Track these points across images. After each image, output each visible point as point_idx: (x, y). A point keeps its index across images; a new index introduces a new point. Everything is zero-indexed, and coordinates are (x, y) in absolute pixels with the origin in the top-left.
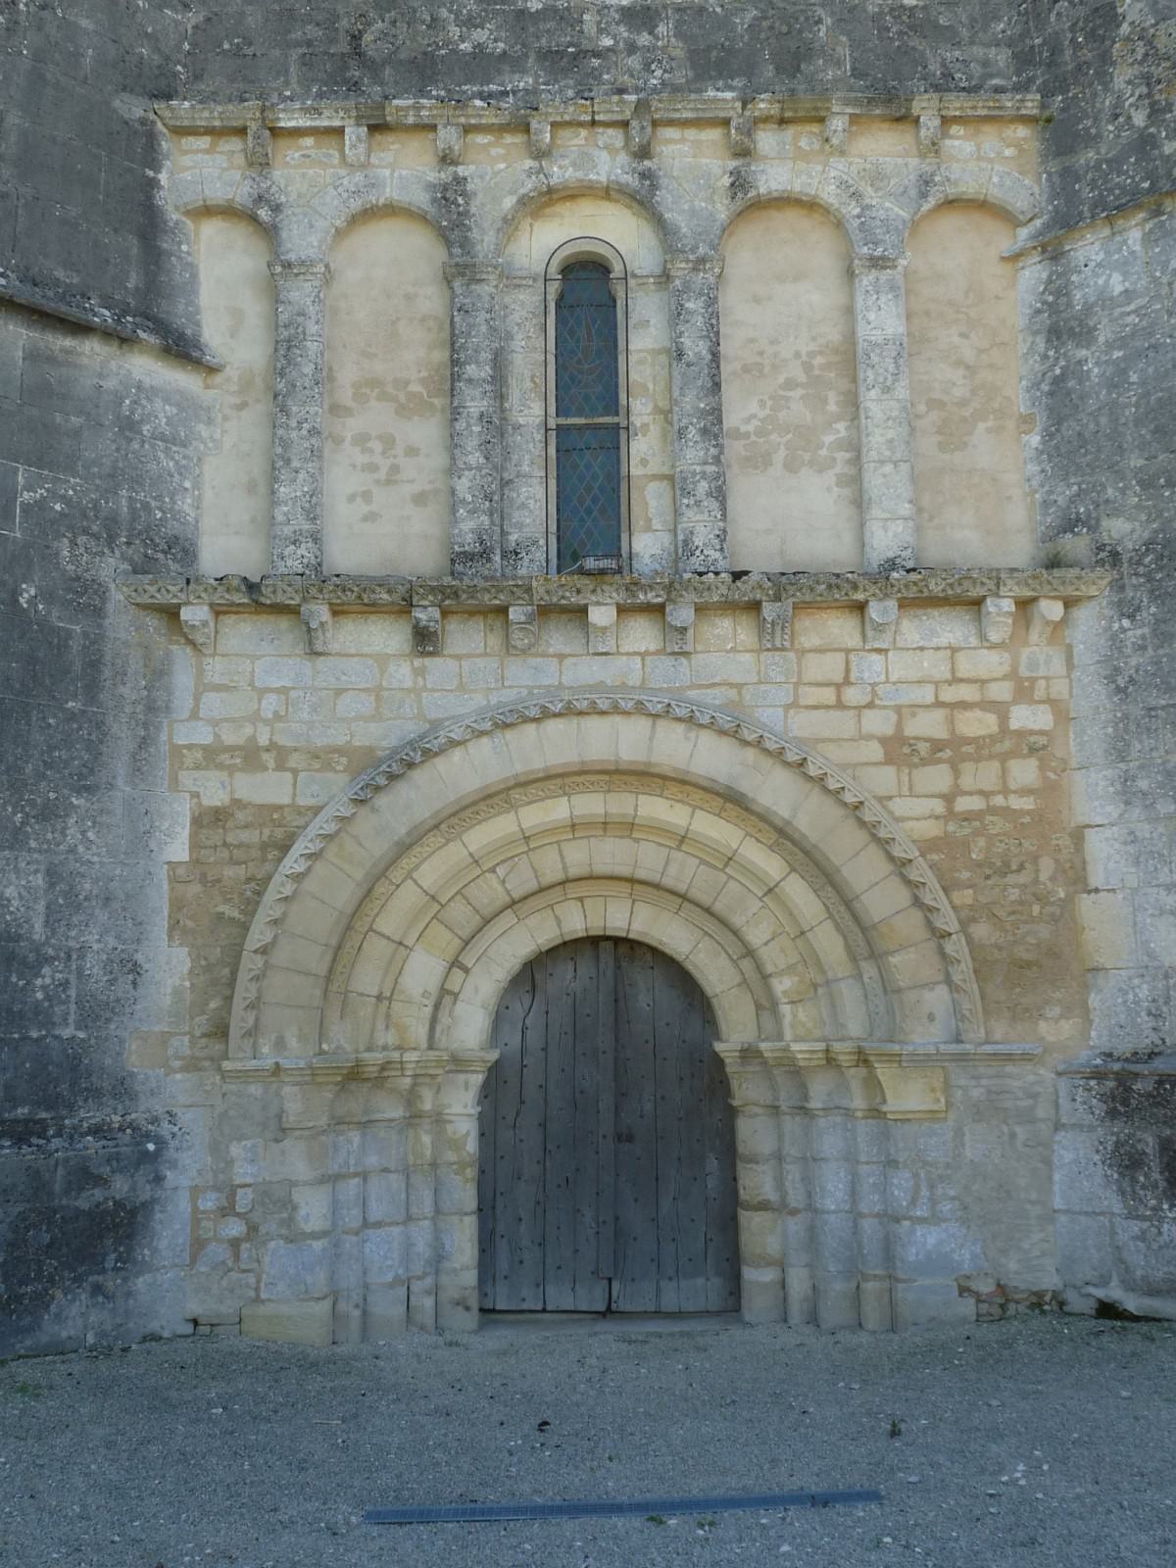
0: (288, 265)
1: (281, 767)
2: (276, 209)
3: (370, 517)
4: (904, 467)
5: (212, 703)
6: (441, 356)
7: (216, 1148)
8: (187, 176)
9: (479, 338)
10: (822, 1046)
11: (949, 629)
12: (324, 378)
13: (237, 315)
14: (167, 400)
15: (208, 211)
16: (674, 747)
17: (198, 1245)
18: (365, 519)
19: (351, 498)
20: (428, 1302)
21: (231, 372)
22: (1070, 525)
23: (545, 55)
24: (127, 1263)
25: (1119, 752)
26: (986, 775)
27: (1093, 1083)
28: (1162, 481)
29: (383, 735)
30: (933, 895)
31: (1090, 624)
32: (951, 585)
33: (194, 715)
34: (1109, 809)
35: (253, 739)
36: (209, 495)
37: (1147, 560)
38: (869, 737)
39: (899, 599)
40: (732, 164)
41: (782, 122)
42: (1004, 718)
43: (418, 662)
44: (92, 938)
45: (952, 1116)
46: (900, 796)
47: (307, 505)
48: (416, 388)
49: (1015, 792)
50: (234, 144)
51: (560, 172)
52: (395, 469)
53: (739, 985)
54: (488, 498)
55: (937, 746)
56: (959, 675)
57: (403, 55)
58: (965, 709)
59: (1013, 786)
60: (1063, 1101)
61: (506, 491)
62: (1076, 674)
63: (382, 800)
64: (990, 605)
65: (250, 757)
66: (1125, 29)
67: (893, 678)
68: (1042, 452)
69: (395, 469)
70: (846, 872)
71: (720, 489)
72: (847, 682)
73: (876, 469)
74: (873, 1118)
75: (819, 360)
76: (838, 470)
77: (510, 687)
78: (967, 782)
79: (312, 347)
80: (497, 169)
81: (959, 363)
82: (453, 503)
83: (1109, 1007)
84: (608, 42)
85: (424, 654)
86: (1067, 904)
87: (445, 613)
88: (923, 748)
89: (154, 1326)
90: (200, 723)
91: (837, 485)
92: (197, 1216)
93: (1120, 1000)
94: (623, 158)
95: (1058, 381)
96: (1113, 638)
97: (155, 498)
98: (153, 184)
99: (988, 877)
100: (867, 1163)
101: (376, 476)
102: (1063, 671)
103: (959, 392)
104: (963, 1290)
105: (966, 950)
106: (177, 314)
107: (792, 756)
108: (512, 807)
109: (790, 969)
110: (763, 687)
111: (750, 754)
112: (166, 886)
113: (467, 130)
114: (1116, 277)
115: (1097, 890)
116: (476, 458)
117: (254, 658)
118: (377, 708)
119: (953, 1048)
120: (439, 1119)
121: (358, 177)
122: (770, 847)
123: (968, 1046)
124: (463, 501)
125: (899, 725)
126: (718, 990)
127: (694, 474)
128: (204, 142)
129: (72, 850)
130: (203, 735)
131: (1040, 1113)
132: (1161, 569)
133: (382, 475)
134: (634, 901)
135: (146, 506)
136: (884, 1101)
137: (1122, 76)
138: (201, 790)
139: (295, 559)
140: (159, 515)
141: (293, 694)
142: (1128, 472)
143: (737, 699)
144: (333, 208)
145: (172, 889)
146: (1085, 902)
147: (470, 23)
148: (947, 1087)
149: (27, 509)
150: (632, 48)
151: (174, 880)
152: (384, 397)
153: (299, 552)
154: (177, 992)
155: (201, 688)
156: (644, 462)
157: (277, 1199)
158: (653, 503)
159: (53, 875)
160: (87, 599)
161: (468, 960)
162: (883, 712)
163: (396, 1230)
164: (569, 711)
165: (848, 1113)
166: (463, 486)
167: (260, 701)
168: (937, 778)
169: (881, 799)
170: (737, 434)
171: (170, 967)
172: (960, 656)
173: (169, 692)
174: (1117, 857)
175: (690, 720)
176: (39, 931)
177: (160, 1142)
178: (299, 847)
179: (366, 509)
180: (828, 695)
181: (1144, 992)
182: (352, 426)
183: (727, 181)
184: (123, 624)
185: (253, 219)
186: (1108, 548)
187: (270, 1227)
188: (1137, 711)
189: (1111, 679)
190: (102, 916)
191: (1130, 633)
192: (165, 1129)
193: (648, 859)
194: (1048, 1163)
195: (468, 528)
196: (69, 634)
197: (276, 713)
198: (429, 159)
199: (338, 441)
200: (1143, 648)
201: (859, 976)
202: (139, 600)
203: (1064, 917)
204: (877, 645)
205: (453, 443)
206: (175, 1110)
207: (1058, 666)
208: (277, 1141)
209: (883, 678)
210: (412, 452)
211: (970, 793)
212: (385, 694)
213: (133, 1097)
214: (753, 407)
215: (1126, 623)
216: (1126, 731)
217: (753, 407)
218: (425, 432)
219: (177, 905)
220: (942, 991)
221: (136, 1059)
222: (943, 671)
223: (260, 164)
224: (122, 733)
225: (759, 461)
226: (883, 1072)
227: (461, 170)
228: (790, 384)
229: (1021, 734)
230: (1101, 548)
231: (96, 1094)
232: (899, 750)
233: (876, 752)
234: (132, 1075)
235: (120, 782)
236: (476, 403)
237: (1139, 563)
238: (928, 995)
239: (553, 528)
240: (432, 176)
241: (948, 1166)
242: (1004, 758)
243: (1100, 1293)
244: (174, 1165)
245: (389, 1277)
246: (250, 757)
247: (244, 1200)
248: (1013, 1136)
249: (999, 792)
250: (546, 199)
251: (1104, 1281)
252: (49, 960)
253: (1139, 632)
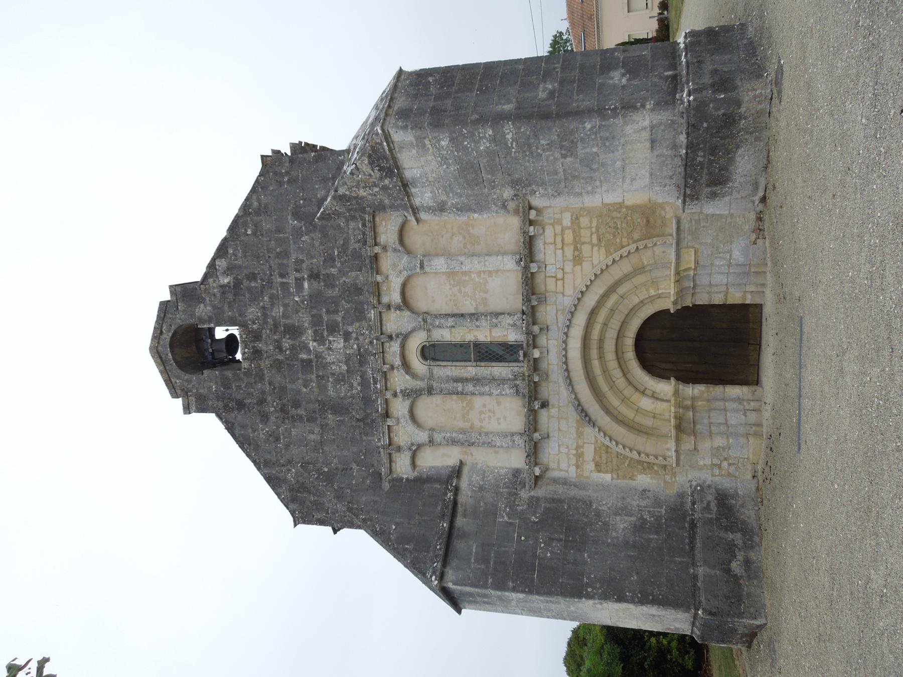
0: (430, 441)
1: (583, 447)
2: (412, 444)
3: (505, 418)
4: (486, 258)
5: (564, 466)
6: (454, 397)
7: (700, 469)
8: (403, 469)
9: (450, 386)
11: (539, 245)
12: (463, 431)
13: (444, 455)
14: (472, 477)
15: (414, 464)
16: (577, 332)
17: (729, 475)
19: (499, 424)
20: (752, 404)
21: (462, 458)
22: (504, 207)
23: (361, 366)
24: (735, 496)
26: (585, 233)
29: (573, 416)
30: (624, 251)
33: (567, 471)
36: (499, 465)
38: (573, 270)
40: (392, 310)
41: (379, 295)
42: (568, 228)
44: (635, 503)
45: (697, 246)
48: (465, 404)
50: (394, 456)
51: (397, 362)
52: (490, 411)
54: (499, 385)
55: (576, 249)
57: (363, 406)
60: (693, 211)
63: (593, 418)
65: (579, 456)
66: (347, 193)
69: (490, 411)
70: (616, 278)
72: (555, 277)
75: (452, 282)
78: (588, 240)
79: (454, 435)
80: (399, 380)
81: (451, 238)
82: (501, 394)
84: (355, 346)
85: (548, 405)
86: (628, 208)
87: (536, 399)
88: (577, 253)
89: (754, 489)
92: (721, 475)
94: (392, 343)
95: (458, 209)
98: (407, 479)
103: (461, 239)
104: (755, 243)
106: (445, 473)
108: (594, 378)
109: (647, 290)
111: (579, 307)
113: (386, 389)
114: (426, 195)
116: (487, 389)
120: (693, 398)
121: (402, 421)
128: (393, 465)
129: (609, 508)
131: (697, 218)
133: (492, 415)
135: (505, 484)
137: (362, 193)
139: (519, 441)
144: (411, 428)
146: (627, 203)
147: (351, 387)
148: (688, 247)
149: (509, 518)
150: (357, 339)
151: (618, 478)
152: (468, 414)
154: (651, 478)
156: (486, 336)
157: (716, 452)
158: (499, 334)
159: (616, 514)
160: (534, 502)
161: (642, 389)
163: (728, 414)
166: (496, 392)
168: (586, 249)
169: (593, 268)
170: (476, 308)
171: (644, 480)
172: (547, 241)
173: (559, 478)
175: (568, 327)
176: (633, 519)
177: (697, 486)
178: (608, 443)
180: (560, 283)
181: (657, 188)
182: (477, 423)
183: (398, 312)
184: (540, 492)
185: (415, 451)
187: (725, 454)
188: (566, 190)
190: (629, 500)
192: (694, 483)
193: (611, 335)
194: (713, 215)
195: (508, 391)
196: (545, 508)
198: (395, 400)
199: (481, 427)
201: (650, 271)
203: (633, 209)
205: (482, 394)
210: (484, 406)
213: (684, 492)
214: (468, 303)
217: (468, 303)
218: (478, 401)
219: (625, 477)
220: (656, 248)
221: (673, 491)
222: (552, 247)
223: (399, 449)
224: (573, 492)
225: (485, 301)
227: (398, 391)
228: (460, 291)
229: (572, 223)
231: (682, 504)
232: (578, 260)
233: (578, 268)
236: (470, 387)
238: (657, 253)
240: (401, 399)
243: (757, 202)
244: (705, 482)
245: (743, 417)
246: (579, 456)
247: (716, 461)
250: (406, 365)
251: (753, 202)
252: (642, 516)
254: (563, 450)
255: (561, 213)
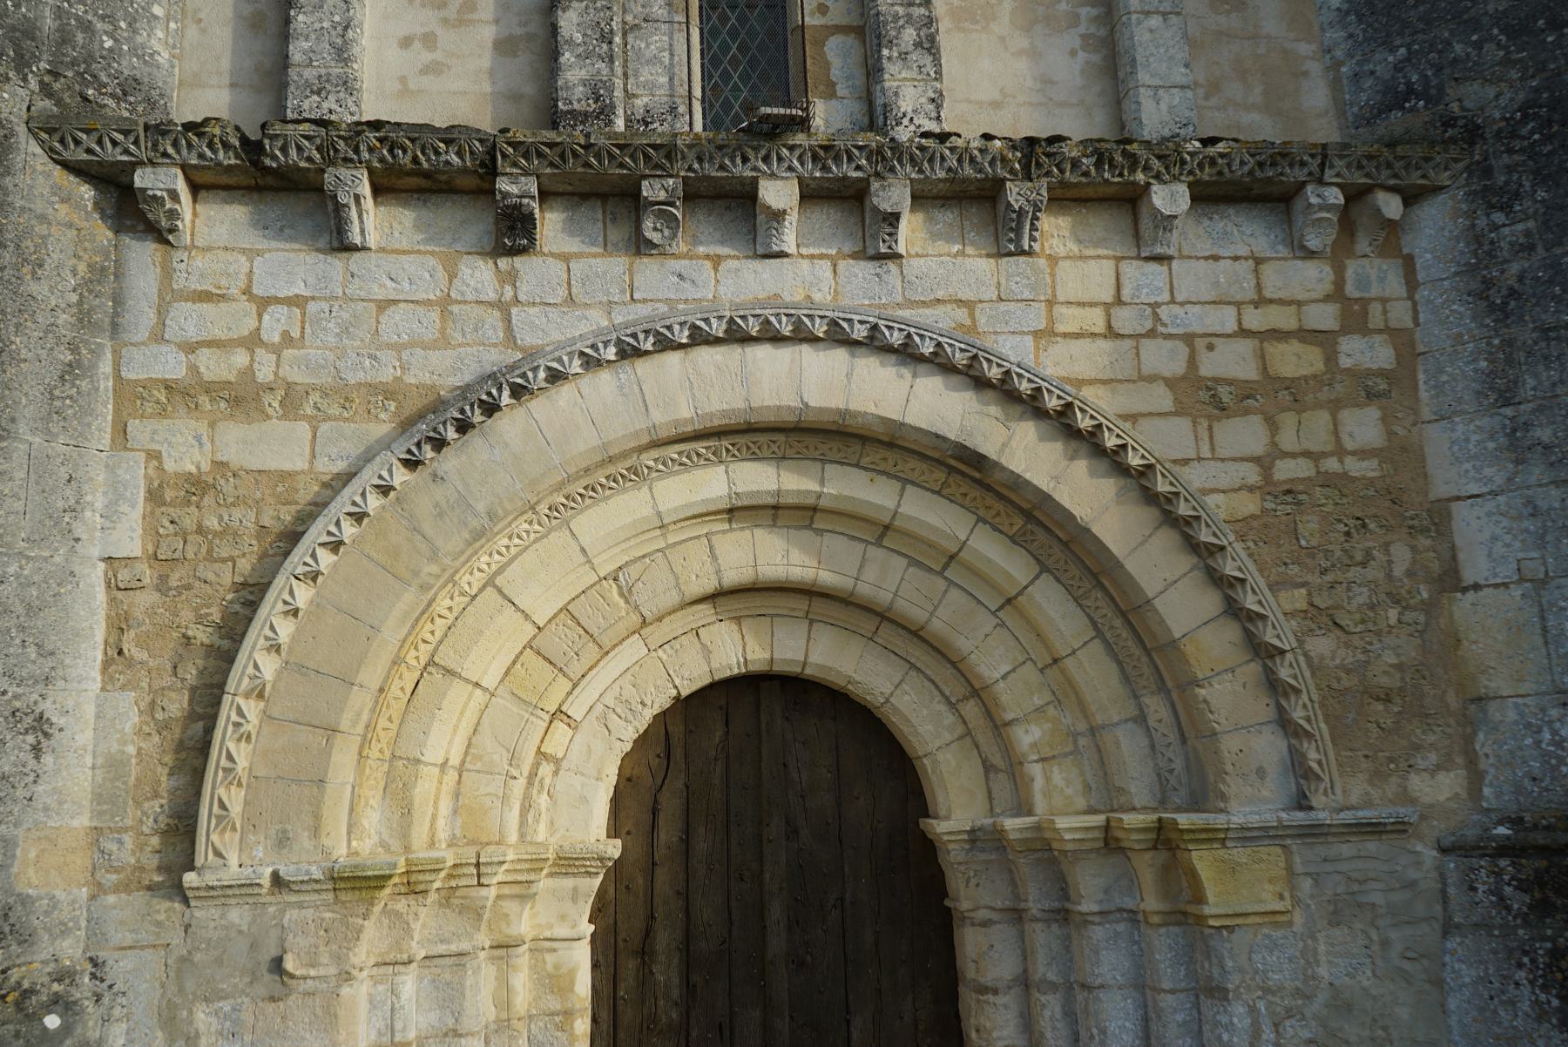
5: (188, 320)
10: (1099, 819)
18: (426, 70)
25: (1500, 391)
27: (1503, 863)
28: (1541, 22)
29: (446, 369)
31: (1436, 229)
32: (1261, 165)
34: (1488, 471)
35: (248, 373)
37: (1524, 131)
38: (1152, 379)
39: (1190, 186)
42: (1331, 357)
43: (503, 263)
46: (1199, 459)
47: (339, 41)
49: (1353, 453)
53: (960, 738)
55: (1246, 392)
56: (1268, 294)
58: (1279, 340)
59: (1349, 444)
61: (630, 39)
62: (1422, 294)
64: (1312, 195)
67: (1179, 298)
68: (1348, 13)
71: (932, 39)
73: (1139, 22)
74: (1179, 924)
76: (1082, 29)
77: (645, 301)
78: (1288, 440)
83: (1511, 752)
90: (164, 348)
91: (1083, 49)
93: (1529, 741)
96: (1478, 239)
97: (102, 18)
99: (1324, 572)
100: (1172, 992)
101: (443, 14)
102: (1403, 292)
105: (1307, 674)
107: (1052, 403)
110: (1003, 307)
112: (101, 596)
115: (1476, 587)
117: (252, 254)
118: (443, 331)
119: (1300, 817)
122: (1012, 539)
123: (1321, 815)
124: (570, 42)
125: (1192, 362)
126: (932, 747)
127: (896, 17)
130: (172, 366)
132: (1548, 139)
134: (811, 624)
135: (87, 27)
136: (1200, 899)
138: (164, 449)
140: (108, 44)
141: (312, 307)
142: (1485, 20)
143: (968, 322)
145: (112, 601)
153: (325, 105)
155: (168, 296)
162: (1169, 344)
164: (736, 336)
165: (1134, 917)
167: (260, 316)
172: (1268, 270)
174: (1508, 539)
179: (427, 57)
186: (1461, 122)
189: (1481, 295)
191: (1506, 231)
197: (286, 335)
200: (1531, 248)
202: (67, 155)
204: (1159, 250)
206: (102, 955)
207: (1395, 285)
208: (273, 999)
209: (1166, 297)
211: (1293, 455)
212: (455, 309)
215: (1499, 217)
216: (1510, 361)
226: (1203, 861)
230: (1450, 122)
234: (25, 900)
235: (22, 427)
237: (1513, 135)
239: (698, 92)
241: (1298, 992)
242: (1335, 406)
246: (241, 399)
248: (1385, 944)
249: (1332, 454)
253: (1520, 227)
254: (275, 323)
255: (1387, 330)
